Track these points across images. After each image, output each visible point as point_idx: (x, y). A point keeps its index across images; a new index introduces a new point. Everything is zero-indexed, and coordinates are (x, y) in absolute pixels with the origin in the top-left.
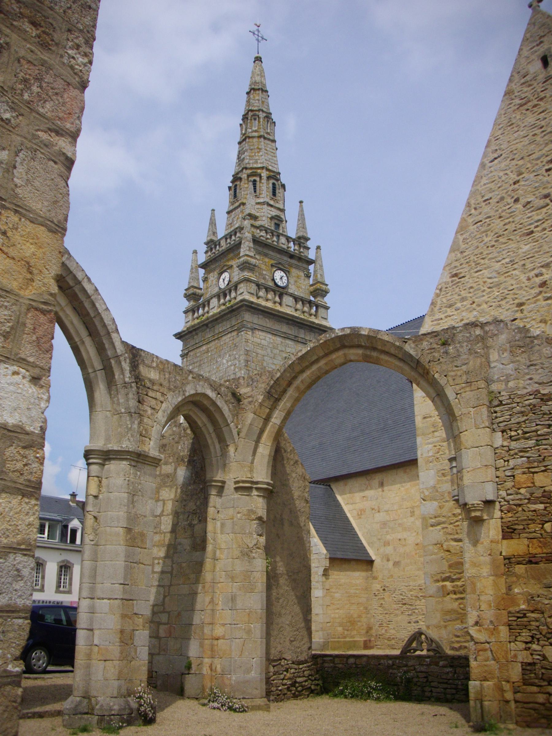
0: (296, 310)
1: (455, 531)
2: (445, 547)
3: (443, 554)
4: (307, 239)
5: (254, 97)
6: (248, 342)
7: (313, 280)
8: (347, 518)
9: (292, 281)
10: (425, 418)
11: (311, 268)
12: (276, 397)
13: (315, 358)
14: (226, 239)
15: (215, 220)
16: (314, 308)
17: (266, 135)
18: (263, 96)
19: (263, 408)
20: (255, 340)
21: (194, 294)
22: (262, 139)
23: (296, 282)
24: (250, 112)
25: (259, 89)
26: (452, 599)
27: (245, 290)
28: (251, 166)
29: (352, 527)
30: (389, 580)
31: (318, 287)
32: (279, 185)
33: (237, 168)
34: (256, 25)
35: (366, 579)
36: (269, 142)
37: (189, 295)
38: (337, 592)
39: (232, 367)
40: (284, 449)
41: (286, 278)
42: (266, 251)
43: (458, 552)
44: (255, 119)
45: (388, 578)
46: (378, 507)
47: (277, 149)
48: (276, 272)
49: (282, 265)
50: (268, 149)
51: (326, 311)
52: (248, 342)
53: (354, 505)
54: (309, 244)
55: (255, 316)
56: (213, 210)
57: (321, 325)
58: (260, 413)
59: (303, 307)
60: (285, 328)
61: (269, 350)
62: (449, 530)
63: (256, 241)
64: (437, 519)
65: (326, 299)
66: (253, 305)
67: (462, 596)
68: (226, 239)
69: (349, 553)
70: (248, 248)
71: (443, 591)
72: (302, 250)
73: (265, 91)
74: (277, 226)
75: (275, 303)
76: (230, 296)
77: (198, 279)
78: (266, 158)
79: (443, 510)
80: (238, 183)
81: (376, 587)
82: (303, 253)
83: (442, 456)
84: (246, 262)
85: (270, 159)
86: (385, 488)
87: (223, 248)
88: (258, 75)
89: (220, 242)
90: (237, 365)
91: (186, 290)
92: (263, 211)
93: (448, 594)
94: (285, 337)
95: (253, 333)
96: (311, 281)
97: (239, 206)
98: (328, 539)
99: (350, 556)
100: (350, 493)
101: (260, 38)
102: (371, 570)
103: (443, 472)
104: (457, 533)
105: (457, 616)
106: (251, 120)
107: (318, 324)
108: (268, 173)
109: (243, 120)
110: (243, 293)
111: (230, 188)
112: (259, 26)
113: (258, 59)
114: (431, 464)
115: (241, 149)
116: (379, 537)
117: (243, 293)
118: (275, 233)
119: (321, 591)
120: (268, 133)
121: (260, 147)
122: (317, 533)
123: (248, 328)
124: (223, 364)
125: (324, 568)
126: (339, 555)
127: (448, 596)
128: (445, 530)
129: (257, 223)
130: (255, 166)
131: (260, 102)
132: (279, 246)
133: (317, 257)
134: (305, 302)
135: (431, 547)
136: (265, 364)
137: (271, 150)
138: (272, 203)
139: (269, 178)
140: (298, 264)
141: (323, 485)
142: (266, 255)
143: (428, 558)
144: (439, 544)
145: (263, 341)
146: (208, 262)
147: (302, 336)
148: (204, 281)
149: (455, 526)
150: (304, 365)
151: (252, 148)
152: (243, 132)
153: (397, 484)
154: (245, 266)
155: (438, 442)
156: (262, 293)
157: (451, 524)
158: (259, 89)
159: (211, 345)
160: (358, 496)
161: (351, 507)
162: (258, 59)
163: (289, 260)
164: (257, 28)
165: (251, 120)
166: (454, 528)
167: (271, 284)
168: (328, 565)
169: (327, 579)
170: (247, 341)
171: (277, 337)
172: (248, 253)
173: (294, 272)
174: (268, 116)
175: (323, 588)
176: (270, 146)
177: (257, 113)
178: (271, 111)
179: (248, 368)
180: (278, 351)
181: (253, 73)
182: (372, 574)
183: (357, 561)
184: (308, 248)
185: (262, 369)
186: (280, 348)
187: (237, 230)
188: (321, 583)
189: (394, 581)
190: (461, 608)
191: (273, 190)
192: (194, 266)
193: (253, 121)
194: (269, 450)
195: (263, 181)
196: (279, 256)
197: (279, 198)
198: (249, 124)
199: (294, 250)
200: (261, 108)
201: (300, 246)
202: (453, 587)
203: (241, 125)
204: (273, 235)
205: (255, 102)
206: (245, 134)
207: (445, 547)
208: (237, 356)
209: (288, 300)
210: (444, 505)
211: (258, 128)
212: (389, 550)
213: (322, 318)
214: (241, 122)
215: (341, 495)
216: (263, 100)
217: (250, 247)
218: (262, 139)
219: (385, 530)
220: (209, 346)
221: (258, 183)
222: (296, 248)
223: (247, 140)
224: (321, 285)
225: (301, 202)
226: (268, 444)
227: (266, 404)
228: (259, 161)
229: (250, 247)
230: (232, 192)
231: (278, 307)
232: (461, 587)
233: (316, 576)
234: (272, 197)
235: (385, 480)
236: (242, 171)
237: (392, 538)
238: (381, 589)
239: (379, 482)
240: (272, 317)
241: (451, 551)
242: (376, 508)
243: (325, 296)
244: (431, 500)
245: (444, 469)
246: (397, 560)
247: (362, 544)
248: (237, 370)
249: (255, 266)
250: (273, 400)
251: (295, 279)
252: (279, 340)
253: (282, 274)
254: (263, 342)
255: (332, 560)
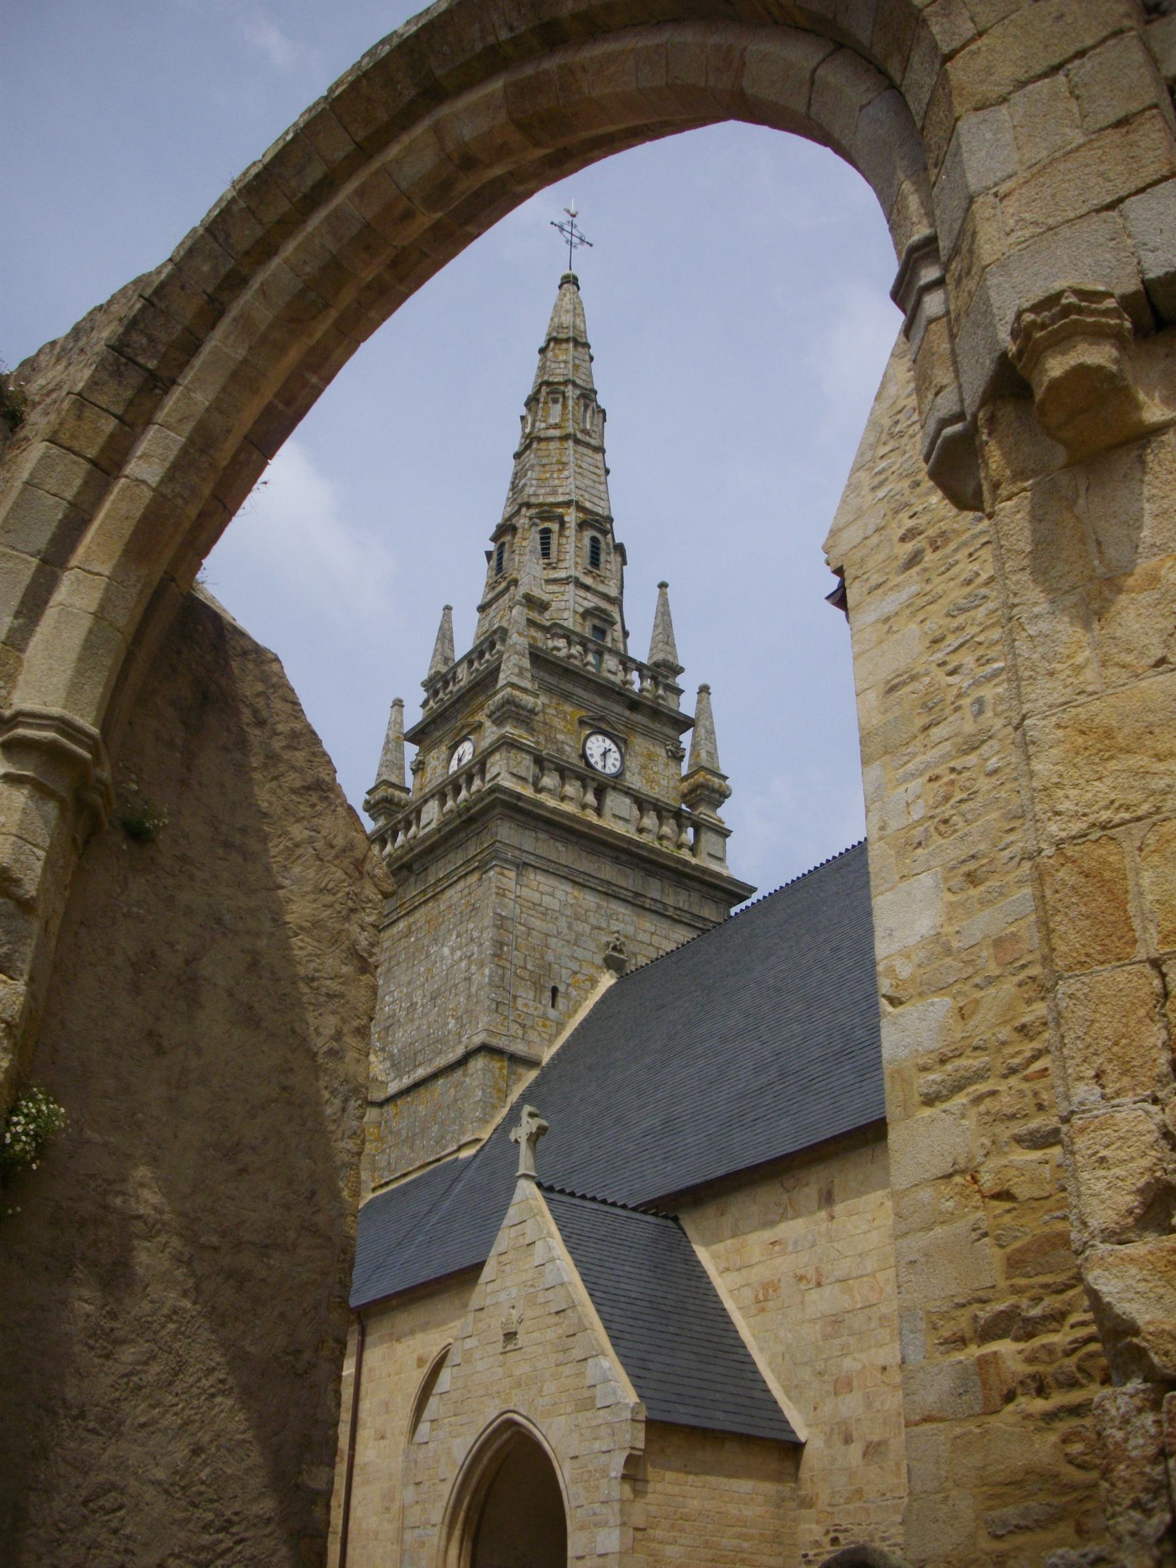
0: (641, 830)
1: (1029, 1099)
2: (987, 1180)
3: (980, 1214)
4: (678, 670)
5: (556, 356)
6: (504, 896)
7: (690, 766)
8: (723, 1313)
9: (633, 764)
10: (891, 690)
11: (686, 739)
12: (152, 364)
13: (315, 172)
14: (471, 663)
15: (451, 629)
16: (691, 831)
17: (579, 435)
18: (576, 354)
19: (90, 413)
20: (525, 892)
21: (388, 800)
22: (571, 443)
23: (644, 767)
24: (544, 388)
25: (567, 340)
26: (1028, 1416)
27: (504, 768)
28: (541, 500)
29: (738, 1338)
30: (851, 1507)
31: (701, 780)
32: (607, 544)
33: (509, 509)
34: (568, 211)
35: (778, 1506)
36: (589, 452)
37: (378, 803)
38: (674, 1542)
39: (463, 964)
40: (255, 712)
41: (617, 755)
42: (568, 687)
43: (1048, 1188)
44: (555, 401)
45: (848, 1501)
46: (817, 1270)
47: (607, 472)
48: (593, 739)
49: (608, 723)
50: (584, 465)
51: (720, 840)
52: (504, 896)
53: (744, 1272)
54: (680, 681)
55: (527, 832)
56: (448, 608)
57: (705, 871)
58: (74, 437)
59: (661, 825)
60: (608, 871)
61: (563, 923)
62: (1005, 1102)
63: (539, 658)
64: (949, 1067)
65: (721, 812)
66: (521, 804)
67: (1075, 1397)
68: (471, 663)
69: (721, 1416)
70: (516, 670)
71: (984, 1383)
72: (661, 692)
73: (580, 343)
74: (600, 632)
75: (584, 806)
76: (469, 789)
77: (402, 768)
78: (578, 483)
79: (972, 1023)
80: (507, 538)
81: (811, 1531)
82: (664, 700)
83: (964, 807)
84: (509, 702)
85: (587, 486)
86: (839, 1208)
87: (462, 684)
88: (567, 311)
89: (455, 673)
90: (475, 956)
91: (369, 793)
92: (565, 598)
93: (1010, 1397)
94: (607, 894)
95: (519, 875)
96: (685, 769)
97: (507, 589)
98: (651, 1365)
99: (720, 1421)
100: (734, 1236)
101: (575, 240)
102: (796, 1478)
103: (971, 866)
104: (1040, 1107)
105: (1055, 1501)
106: (546, 403)
107: (696, 868)
108: (581, 515)
109: (527, 404)
110: (498, 774)
111: (489, 555)
112: (574, 216)
113: (570, 280)
114: (919, 851)
115: (519, 467)
116: (820, 1366)
117: (498, 774)
118: (590, 646)
119: (616, 1533)
120: (584, 431)
121: (564, 459)
122: (613, 1345)
123: (506, 861)
124: (443, 958)
125: (625, 1454)
126: (683, 1415)
127: (1011, 1407)
128: (987, 1104)
129: (545, 619)
130: (551, 499)
131: (570, 366)
132: (599, 677)
133: (699, 711)
134: (665, 813)
135: (926, 1194)
136: (550, 957)
137: (592, 469)
138: (588, 581)
139: (582, 526)
140: (652, 726)
141: (654, 1214)
142: (566, 696)
143: (917, 1242)
144: (962, 1172)
145: (546, 899)
146: (428, 725)
147: (657, 896)
148: (415, 772)
149: (1026, 1079)
150: (271, 216)
151: (545, 461)
152: (527, 431)
153: (874, 1190)
154: (510, 712)
155: (949, 756)
156: (549, 781)
157: (1013, 1071)
158: (567, 340)
159: (417, 915)
160: (757, 1240)
161: (735, 1278)
162: (570, 280)
163: (627, 713)
164: (570, 219)
165: (546, 403)
166: (1025, 1086)
167: (575, 759)
168: (641, 1445)
169: (638, 1493)
170: (502, 893)
171: (587, 891)
172: (515, 680)
173: (640, 744)
174: (588, 396)
175: (623, 1524)
176: (589, 460)
177: (562, 388)
178: (596, 387)
179: (502, 963)
180: (588, 928)
181: (557, 309)
182: (799, 1488)
183: (746, 1440)
184: (679, 692)
185: (540, 967)
186: (592, 920)
187: (496, 637)
188: (617, 1506)
189: (867, 1510)
190: (1070, 1460)
191: (592, 552)
192: (392, 736)
193: (550, 405)
194: (98, 595)
195: (567, 533)
196: (599, 701)
197: (608, 574)
198: (540, 413)
199: (641, 690)
200: (571, 377)
201: (656, 684)
202: (1031, 1360)
203: (523, 418)
204: (586, 650)
205: (557, 365)
206: (530, 433)
207: (987, 1180)
208: (476, 934)
209: (616, 803)
210: (977, 1002)
211: (563, 420)
212: (850, 1405)
213: (710, 855)
214: (524, 412)
215: (706, 1244)
216: (577, 362)
217: (521, 669)
218: (571, 443)
219: (837, 1341)
220: (411, 919)
221: (554, 537)
222: (648, 683)
223: (535, 445)
224: (709, 777)
225: (663, 586)
226: (96, 567)
227: (103, 400)
228: (560, 490)
229: (521, 669)
230: (494, 563)
231: (593, 818)
232: (1068, 1353)
233: (605, 1481)
234: (590, 568)
235: (836, 1181)
236: (518, 511)
237: (859, 1366)
238: (826, 1540)
239: (820, 1190)
240: (574, 839)
241: (1015, 1191)
242: (811, 1273)
243: (718, 804)
244: (921, 995)
245: (973, 857)
246: (876, 1439)
247: (768, 1391)
248: (473, 968)
249: (532, 711)
250: (134, 379)
251: (641, 760)
252: (590, 900)
253: (608, 743)
254: (546, 899)
255: (657, 1428)
